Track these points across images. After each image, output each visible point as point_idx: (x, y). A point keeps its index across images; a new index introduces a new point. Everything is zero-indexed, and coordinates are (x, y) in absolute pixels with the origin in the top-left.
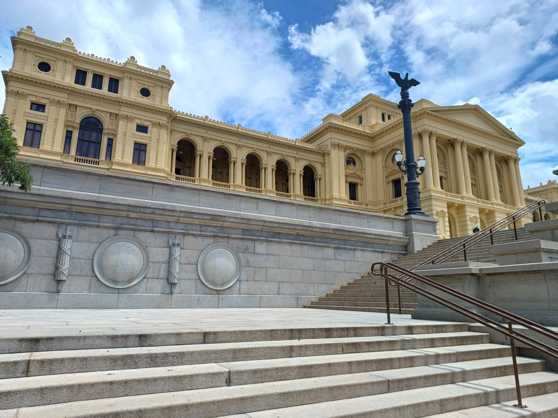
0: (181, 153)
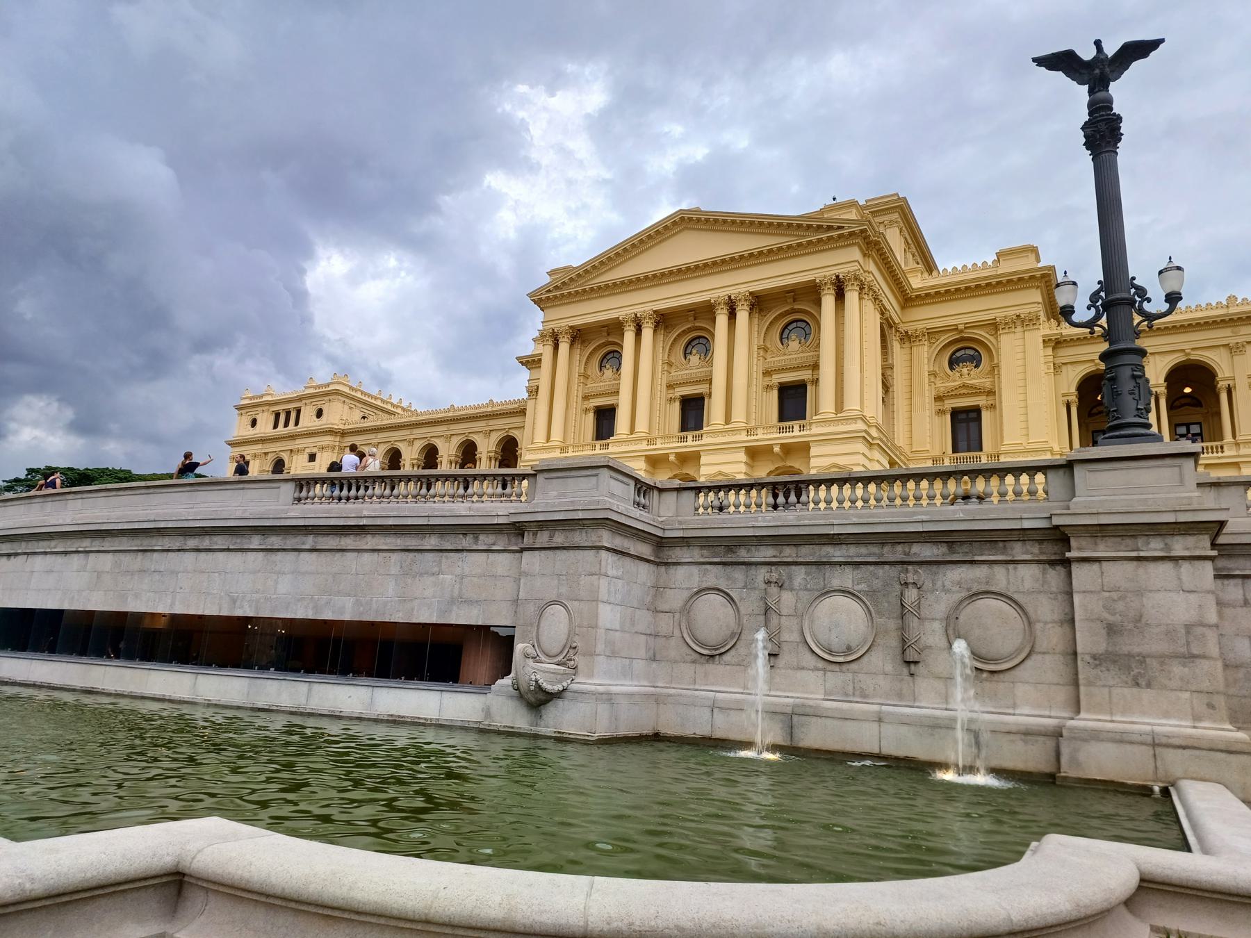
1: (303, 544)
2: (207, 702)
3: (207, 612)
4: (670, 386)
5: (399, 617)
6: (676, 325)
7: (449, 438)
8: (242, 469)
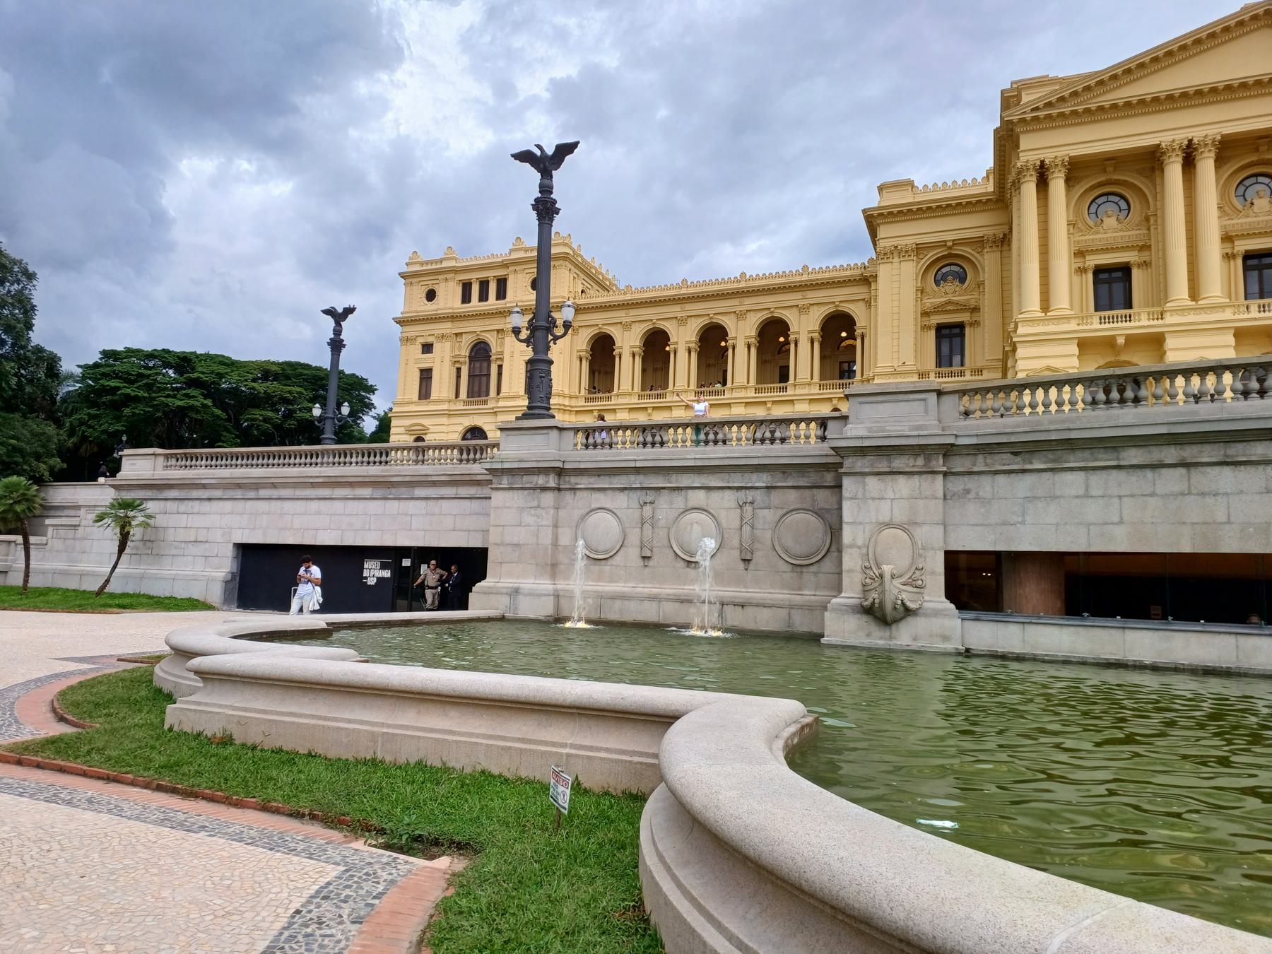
0: (782, 339)
4: (1080, 254)
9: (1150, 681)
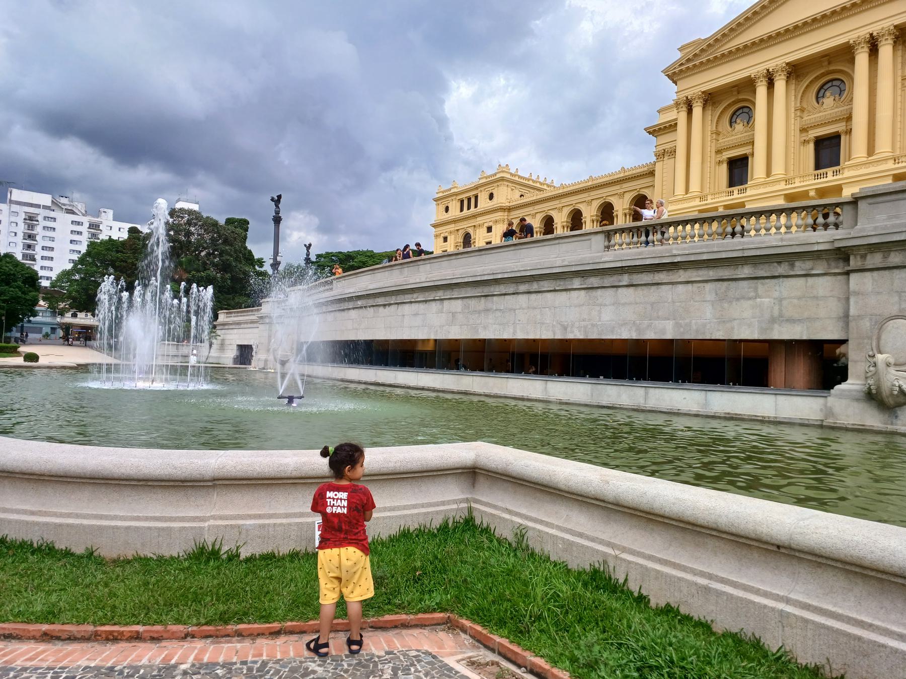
1: (620, 281)
2: (558, 401)
3: (544, 337)
5: (719, 334)
6: (808, 73)
7: (590, 203)
8: (467, 240)
9: (513, 403)
